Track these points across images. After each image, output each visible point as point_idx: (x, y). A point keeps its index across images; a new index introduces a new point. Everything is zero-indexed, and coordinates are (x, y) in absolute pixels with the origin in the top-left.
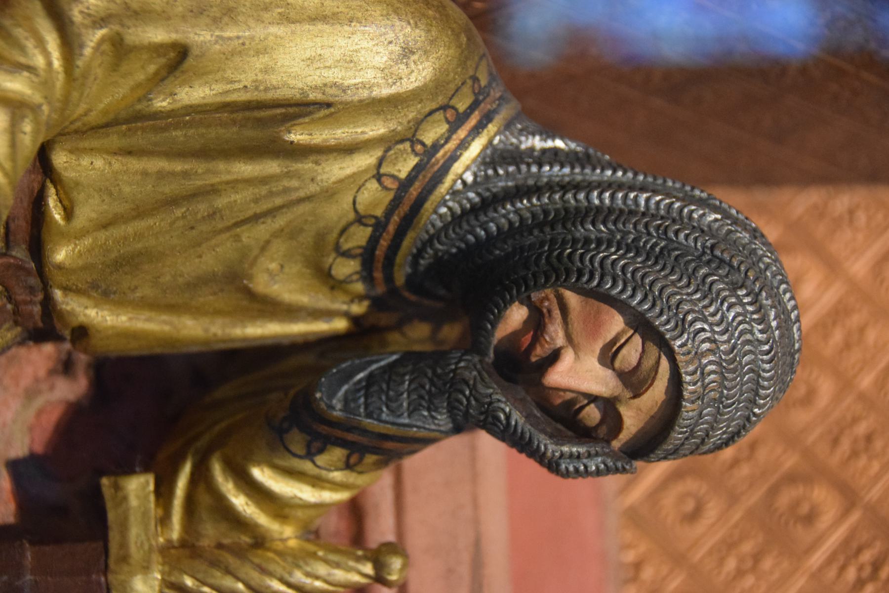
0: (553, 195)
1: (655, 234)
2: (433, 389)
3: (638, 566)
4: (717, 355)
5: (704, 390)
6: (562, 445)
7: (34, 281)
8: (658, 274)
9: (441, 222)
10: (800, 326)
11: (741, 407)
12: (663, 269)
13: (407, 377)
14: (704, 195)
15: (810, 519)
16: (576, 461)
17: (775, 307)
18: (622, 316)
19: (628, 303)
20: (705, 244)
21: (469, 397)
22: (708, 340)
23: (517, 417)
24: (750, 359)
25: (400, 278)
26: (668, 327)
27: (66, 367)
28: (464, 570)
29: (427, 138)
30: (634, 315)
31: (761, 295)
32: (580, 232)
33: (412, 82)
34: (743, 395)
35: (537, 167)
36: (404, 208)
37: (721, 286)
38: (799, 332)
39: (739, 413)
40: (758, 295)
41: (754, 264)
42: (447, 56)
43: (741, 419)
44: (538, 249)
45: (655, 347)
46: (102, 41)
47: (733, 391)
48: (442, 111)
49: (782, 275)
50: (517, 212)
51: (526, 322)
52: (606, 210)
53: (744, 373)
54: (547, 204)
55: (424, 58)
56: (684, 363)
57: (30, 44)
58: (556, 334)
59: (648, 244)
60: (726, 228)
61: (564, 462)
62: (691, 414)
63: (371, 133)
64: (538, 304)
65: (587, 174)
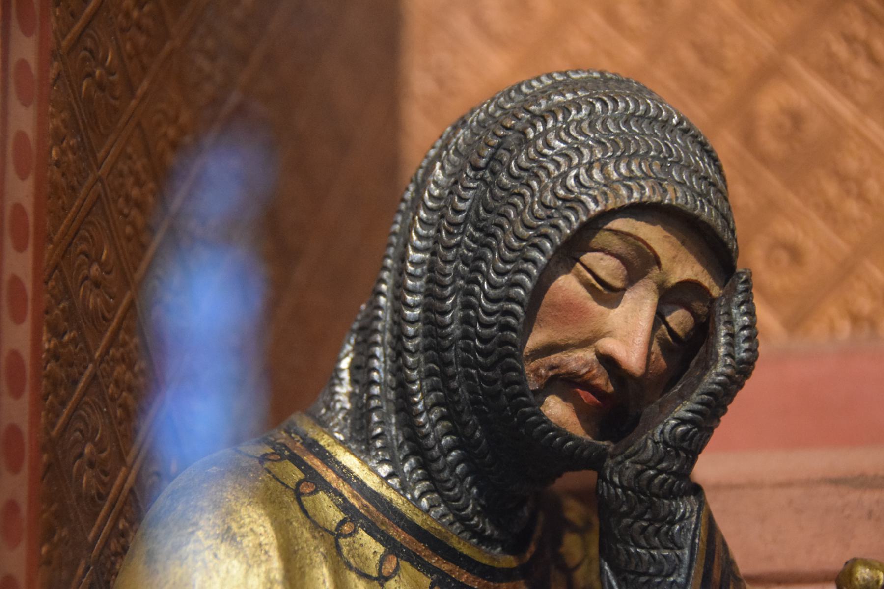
0: (409, 364)
1: (459, 238)
2: (647, 517)
4: (608, 161)
5: (651, 177)
6: (717, 354)
8: (508, 232)
9: (439, 505)
10: (572, 71)
11: (670, 136)
12: (502, 227)
13: (632, 550)
14: (412, 188)
15: (796, 118)
16: (736, 339)
17: (549, 96)
18: (559, 276)
19: (543, 267)
20: (471, 178)
21: (658, 470)
22: (589, 171)
23: (682, 411)
24: (613, 123)
25: (508, 561)
26: (573, 219)
29: (335, 518)
30: (558, 262)
31: (535, 111)
32: (455, 329)
33: (265, 531)
34: (656, 134)
35: (374, 387)
36: (421, 548)
37: (523, 157)
38: (579, 72)
39: (678, 140)
40: (534, 115)
41: (497, 122)
42: (234, 488)
43: (686, 139)
44: (475, 382)
45: (598, 236)
47: (651, 144)
48: (302, 498)
49: (510, 91)
50: (428, 410)
52: (427, 300)
53: (630, 132)
54: (419, 372)
55: (235, 516)
56: (618, 199)
59: (471, 246)
60: (452, 156)
61: (739, 354)
62: (679, 194)
63: (327, 584)
64: (543, 381)
65: (384, 327)
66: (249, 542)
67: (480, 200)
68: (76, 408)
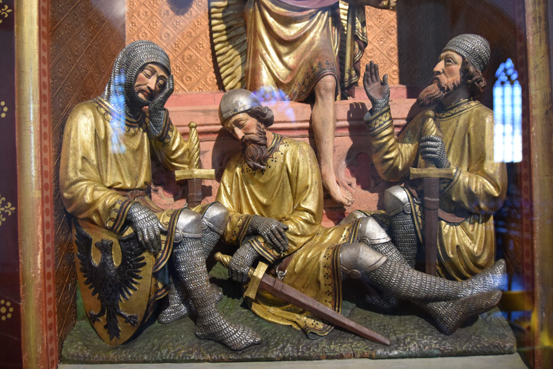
3: (200, 89)
7: (135, 191)
15: (191, 56)
23: (161, 96)
27: (156, 191)
28: (195, 113)
46: (81, 174)
51: (142, 94)
57: (81, 188)
58: (144, 87)
66: (88, 115)
67: (127, 60)
68: (58, 93)
